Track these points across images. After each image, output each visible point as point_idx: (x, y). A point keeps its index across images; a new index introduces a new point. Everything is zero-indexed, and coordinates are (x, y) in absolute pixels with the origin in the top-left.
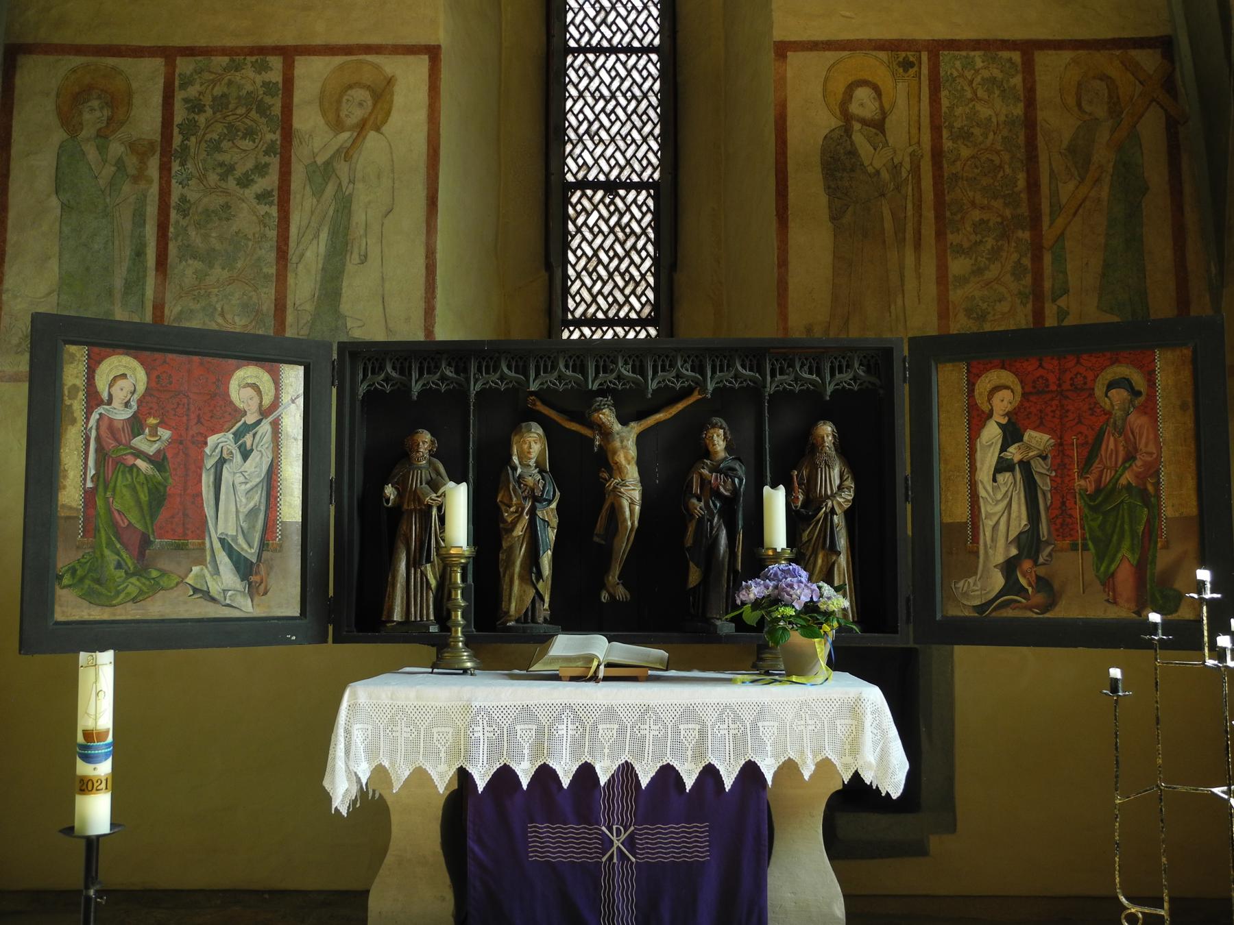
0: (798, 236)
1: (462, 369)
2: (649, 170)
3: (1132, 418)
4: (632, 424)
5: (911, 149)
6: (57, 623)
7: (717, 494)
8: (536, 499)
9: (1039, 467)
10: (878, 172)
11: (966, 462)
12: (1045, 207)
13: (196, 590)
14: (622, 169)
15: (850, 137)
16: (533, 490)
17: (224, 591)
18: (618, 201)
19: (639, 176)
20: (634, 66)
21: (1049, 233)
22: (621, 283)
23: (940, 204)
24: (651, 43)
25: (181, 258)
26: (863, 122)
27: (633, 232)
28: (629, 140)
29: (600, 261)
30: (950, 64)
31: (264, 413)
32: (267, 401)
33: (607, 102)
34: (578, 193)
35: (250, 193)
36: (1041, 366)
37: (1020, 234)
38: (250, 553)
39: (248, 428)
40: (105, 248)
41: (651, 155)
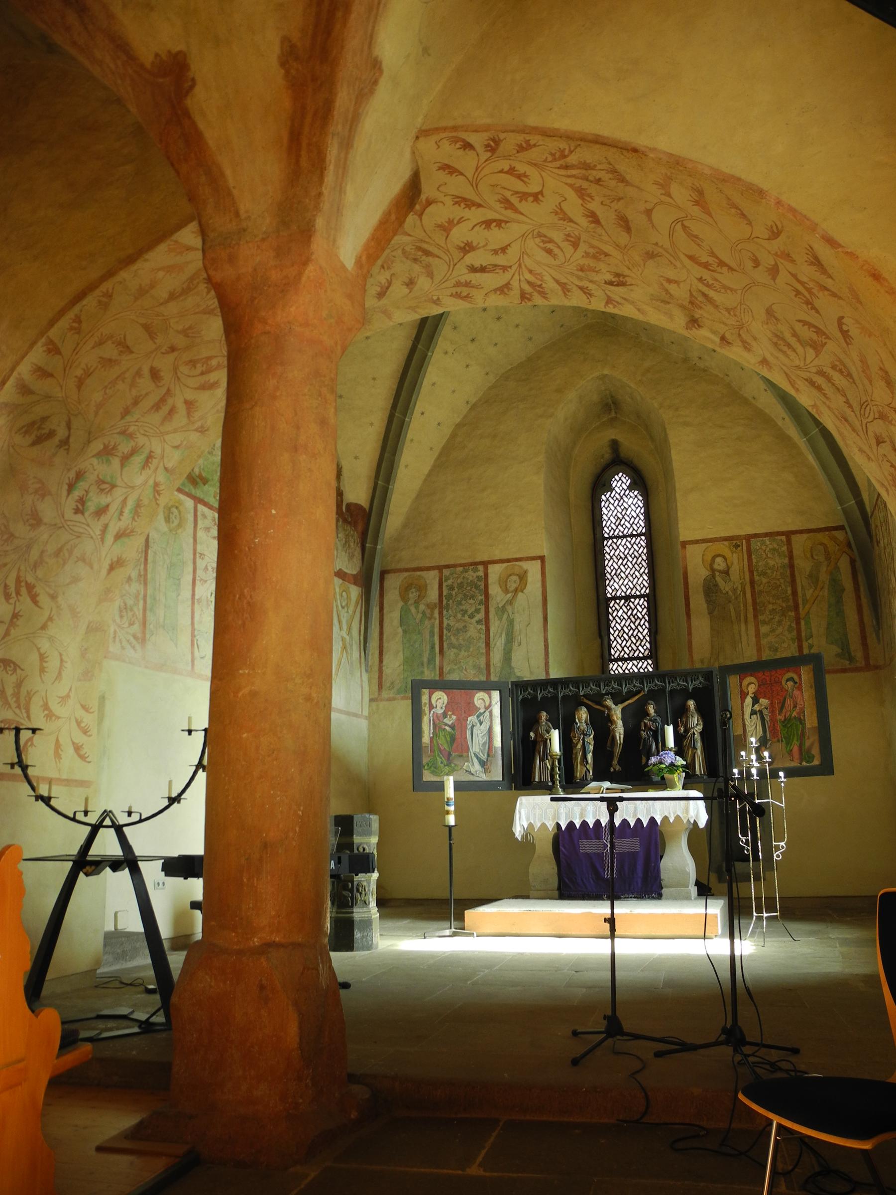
0: (695, 622)
1: (556, 688)
2: (644, 589)
3: (795, 692)
4: (619, 705)
5: (740, 582)
6: (424, 781)
7: (650, 729)
8: (585, 735)
9: (765, 712)
10: (727, 592)
11: (741, 712)
12: (800, 601)
13: (466, 771)
14: (632, 589)
15: (715, 578)
16: (583, 731)
17: (476, 771)
18: (631, 604)
19: (640, 592)
20: (634, 543)
21: (802, 612)
22: (634, 641)
23: (754, 603)
24: (641, 531)
25: (449, 649)
26: (720, 571)
27: (638, 617)
28: (634, 576)
29: (624, 632)
30: (755, 544)
31: (486, 708)
32: (487, 704)
33: (623, 560)
34: (613, 602)
35: (474, 621)
36: (764, 674)
37: (790, 613)
38: (484, 758)
39: (481, 714)
40: (420, 646)
41: (644, 582)
